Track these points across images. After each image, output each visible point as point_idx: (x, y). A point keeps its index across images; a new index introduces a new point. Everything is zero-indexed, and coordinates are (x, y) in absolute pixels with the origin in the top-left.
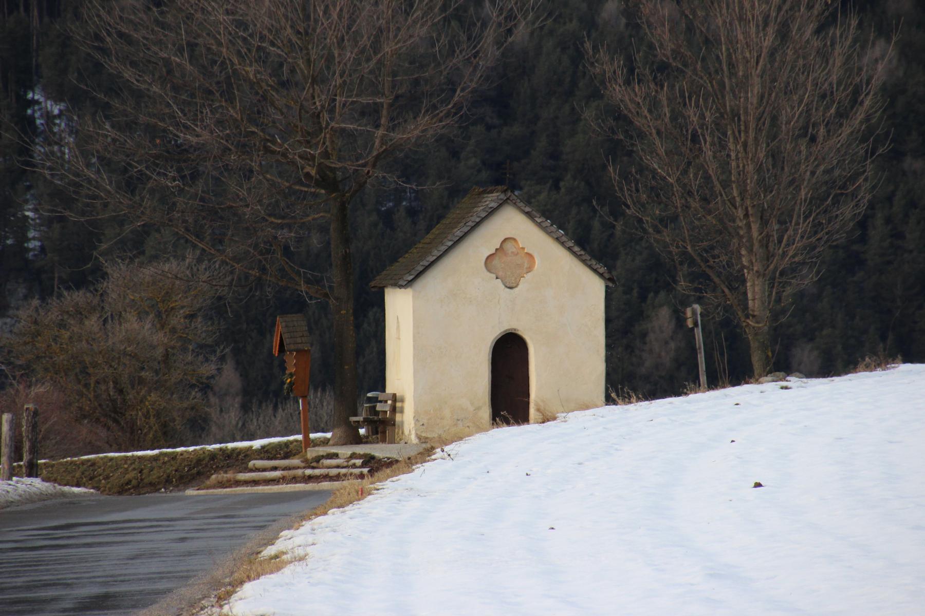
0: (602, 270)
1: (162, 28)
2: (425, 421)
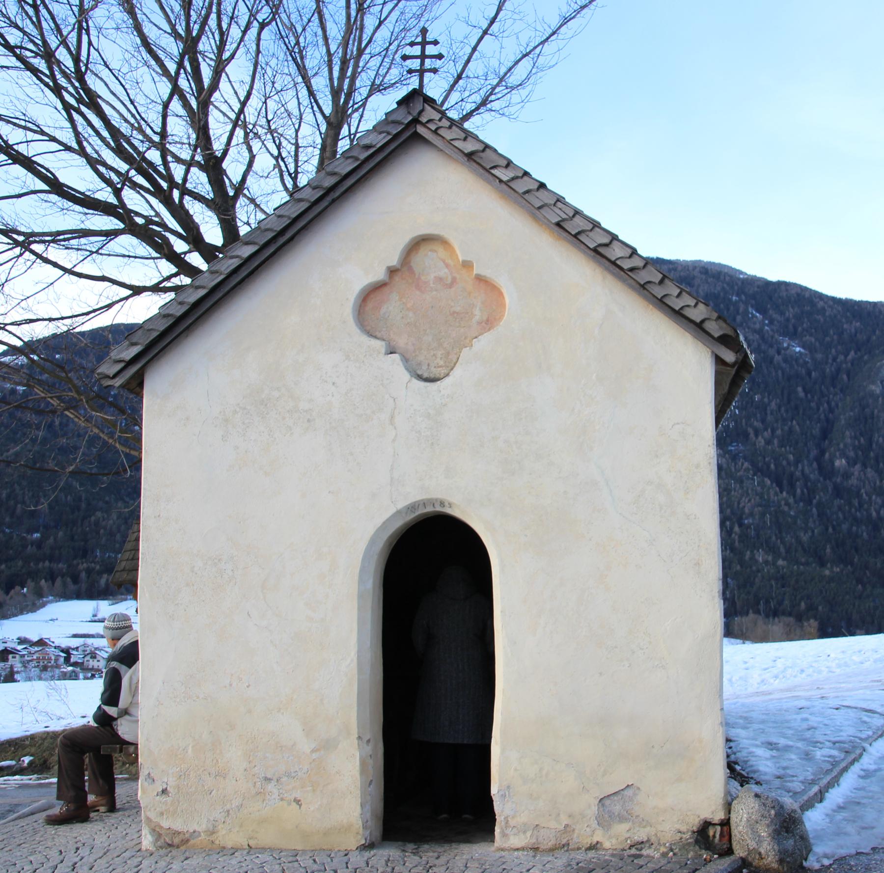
0: (698, 313)
1: (819, 516)
2: (172, 783)
